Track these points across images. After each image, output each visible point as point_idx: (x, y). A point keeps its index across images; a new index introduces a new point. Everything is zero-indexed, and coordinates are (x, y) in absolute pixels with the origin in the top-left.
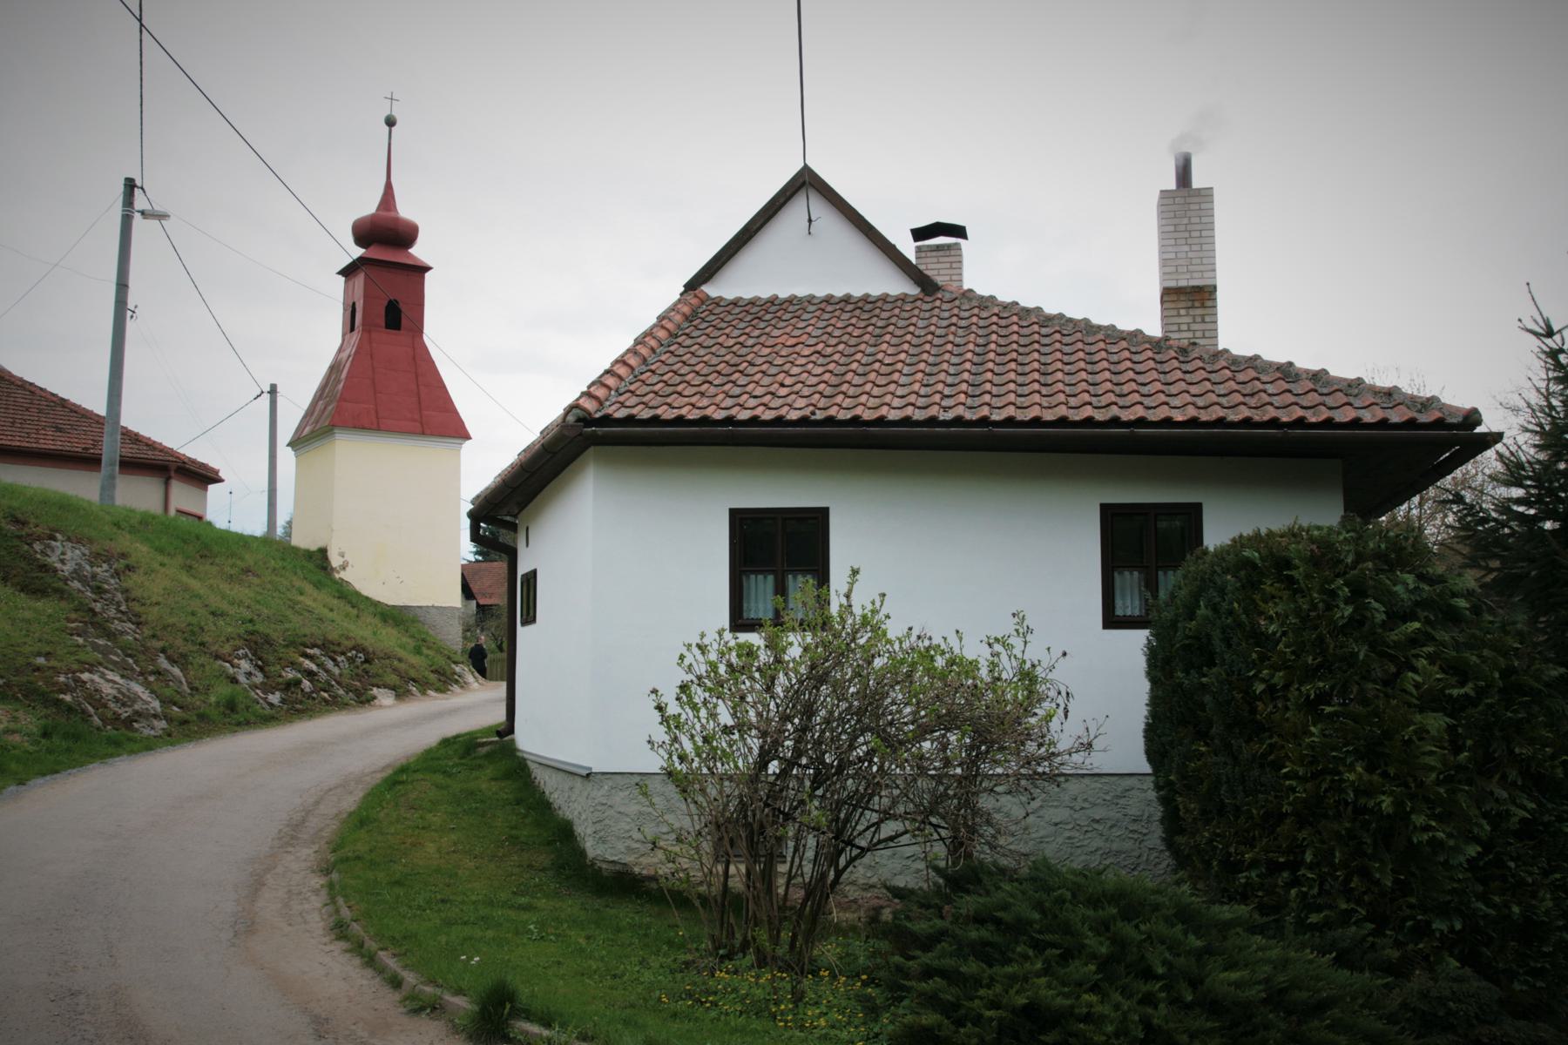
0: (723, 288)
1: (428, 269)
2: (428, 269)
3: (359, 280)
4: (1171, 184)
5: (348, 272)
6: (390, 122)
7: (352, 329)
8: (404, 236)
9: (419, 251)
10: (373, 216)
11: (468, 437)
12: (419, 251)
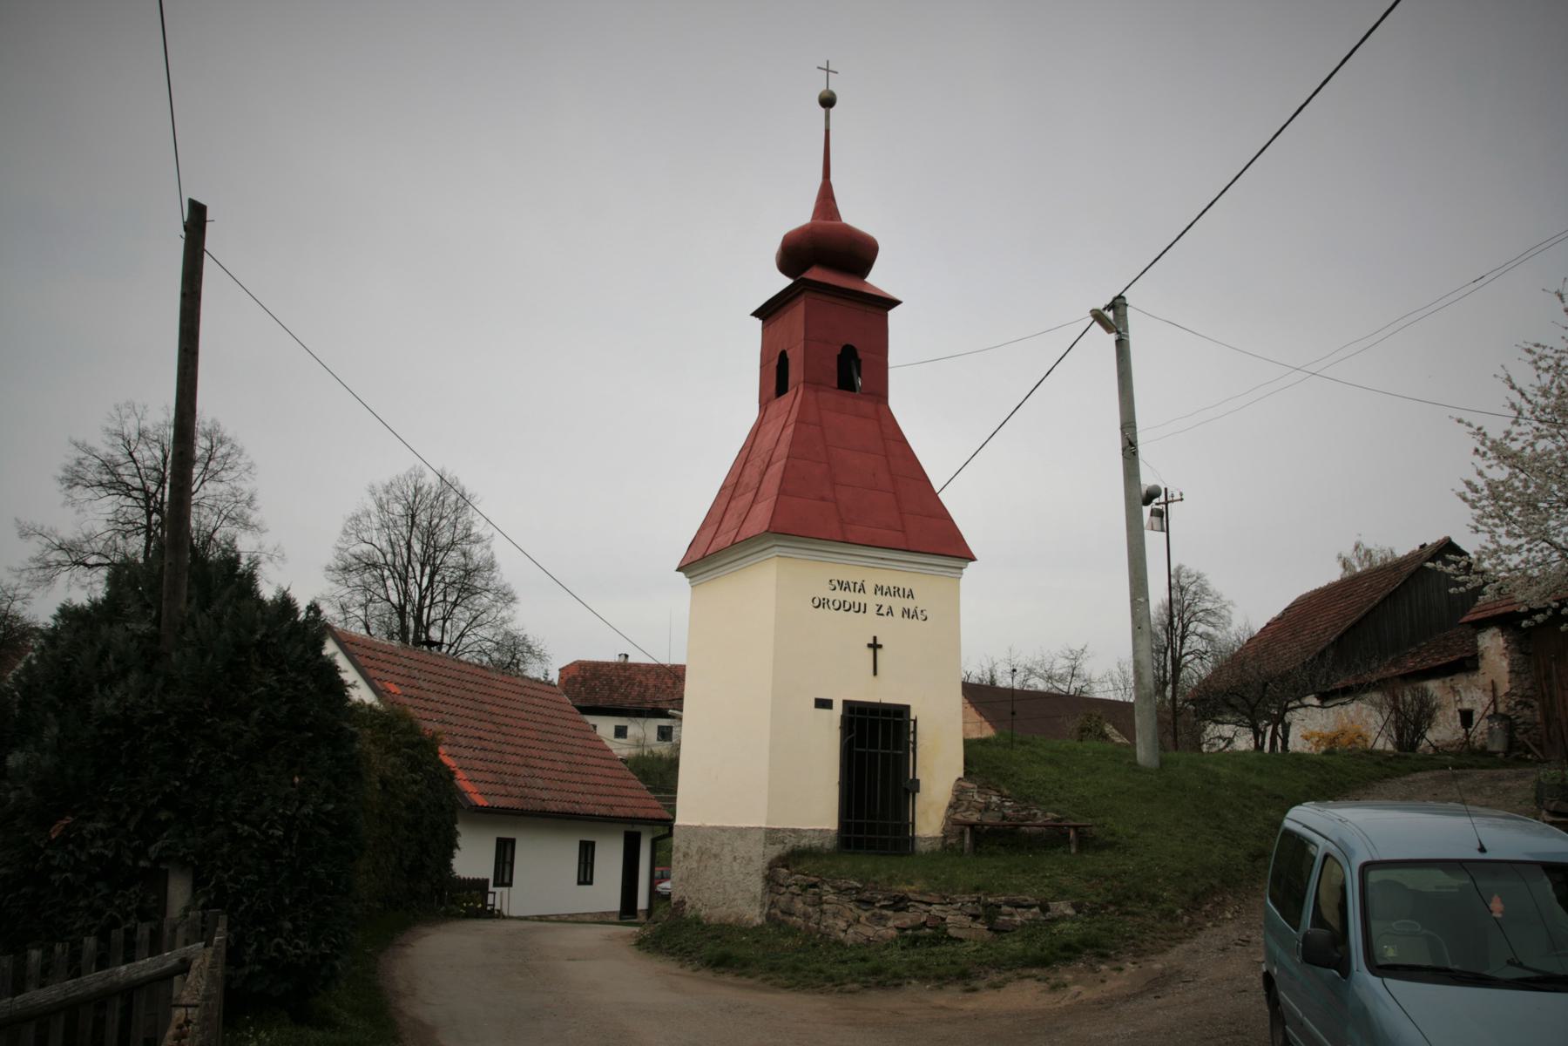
1: (895, 303)
2: (895, 303)
5: (766, 313)
6: (828, 102)
7: (782, 388)
8: (856, 253)
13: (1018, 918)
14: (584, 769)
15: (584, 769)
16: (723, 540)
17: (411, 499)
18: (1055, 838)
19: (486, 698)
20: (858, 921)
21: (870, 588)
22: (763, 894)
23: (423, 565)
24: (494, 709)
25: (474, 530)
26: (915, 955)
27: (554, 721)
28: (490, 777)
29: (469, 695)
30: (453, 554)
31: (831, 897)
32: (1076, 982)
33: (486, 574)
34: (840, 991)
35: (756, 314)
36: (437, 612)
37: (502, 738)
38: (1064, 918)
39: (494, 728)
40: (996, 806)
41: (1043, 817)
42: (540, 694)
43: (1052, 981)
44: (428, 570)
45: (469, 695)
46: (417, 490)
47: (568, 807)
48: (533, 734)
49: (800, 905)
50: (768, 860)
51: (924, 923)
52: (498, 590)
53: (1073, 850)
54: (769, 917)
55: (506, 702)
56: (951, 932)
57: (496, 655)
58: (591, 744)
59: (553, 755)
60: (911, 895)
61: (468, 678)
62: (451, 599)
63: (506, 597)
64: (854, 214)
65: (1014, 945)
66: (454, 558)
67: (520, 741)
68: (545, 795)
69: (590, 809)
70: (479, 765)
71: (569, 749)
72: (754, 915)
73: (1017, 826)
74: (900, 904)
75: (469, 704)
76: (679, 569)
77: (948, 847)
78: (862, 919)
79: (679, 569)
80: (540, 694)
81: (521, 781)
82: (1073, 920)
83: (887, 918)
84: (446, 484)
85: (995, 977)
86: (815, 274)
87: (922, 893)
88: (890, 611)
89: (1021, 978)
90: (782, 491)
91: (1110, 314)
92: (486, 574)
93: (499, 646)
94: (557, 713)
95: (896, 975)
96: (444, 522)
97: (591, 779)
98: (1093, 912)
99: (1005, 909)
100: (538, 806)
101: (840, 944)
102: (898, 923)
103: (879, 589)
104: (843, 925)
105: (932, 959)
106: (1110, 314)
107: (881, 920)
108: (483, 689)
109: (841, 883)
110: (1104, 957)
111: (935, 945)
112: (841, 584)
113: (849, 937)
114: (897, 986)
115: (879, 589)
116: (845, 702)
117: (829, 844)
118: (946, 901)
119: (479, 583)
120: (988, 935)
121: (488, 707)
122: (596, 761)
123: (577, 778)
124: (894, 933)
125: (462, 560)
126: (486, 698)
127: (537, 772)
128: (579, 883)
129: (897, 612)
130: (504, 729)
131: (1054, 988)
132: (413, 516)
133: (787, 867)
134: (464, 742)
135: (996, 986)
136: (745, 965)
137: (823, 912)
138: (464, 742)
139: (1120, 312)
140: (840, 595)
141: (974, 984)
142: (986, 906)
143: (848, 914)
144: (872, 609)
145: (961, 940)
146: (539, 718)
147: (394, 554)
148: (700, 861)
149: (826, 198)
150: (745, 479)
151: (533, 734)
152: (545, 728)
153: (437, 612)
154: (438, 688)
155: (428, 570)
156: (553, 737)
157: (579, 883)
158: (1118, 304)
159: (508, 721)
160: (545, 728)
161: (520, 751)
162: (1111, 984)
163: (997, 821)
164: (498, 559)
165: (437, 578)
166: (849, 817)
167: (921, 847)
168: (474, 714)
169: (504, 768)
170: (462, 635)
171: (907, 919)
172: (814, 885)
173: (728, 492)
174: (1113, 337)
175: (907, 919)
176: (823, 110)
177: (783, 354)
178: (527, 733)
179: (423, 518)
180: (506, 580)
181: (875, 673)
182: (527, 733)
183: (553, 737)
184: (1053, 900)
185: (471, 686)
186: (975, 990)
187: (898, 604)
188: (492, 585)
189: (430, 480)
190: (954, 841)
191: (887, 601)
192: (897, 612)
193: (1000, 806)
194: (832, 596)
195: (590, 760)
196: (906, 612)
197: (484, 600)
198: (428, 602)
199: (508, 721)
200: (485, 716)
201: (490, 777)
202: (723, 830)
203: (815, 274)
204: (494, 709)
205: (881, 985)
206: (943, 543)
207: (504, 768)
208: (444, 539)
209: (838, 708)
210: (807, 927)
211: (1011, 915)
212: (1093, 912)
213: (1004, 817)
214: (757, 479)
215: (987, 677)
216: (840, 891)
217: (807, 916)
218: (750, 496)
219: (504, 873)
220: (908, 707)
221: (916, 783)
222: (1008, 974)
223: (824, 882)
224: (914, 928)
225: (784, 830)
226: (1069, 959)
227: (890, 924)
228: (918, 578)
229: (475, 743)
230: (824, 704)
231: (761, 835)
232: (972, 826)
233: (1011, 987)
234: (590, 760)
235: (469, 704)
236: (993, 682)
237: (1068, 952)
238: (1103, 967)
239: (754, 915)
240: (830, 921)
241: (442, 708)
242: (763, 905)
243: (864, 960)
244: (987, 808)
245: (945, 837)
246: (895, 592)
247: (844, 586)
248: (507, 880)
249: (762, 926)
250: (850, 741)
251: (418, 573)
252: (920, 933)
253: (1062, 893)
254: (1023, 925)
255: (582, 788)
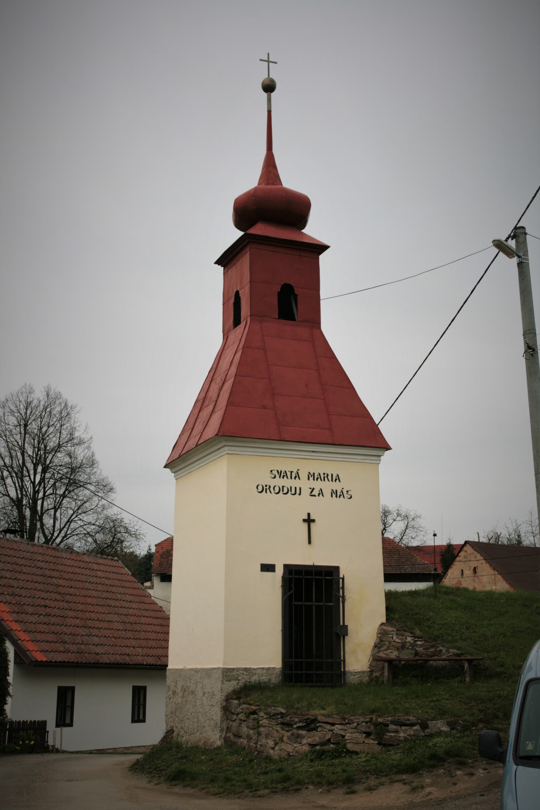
0: (518, 226)
1: (325, 248)
2: (325, 248)
3: (244, 262)
4: (346, 637)
5: (226, 260)
6: (269, 87)
7: (237, 322)
8: (296, 210)
9: (313, 230)
10: (255, 189)
11: (387, 448)
12: (313, 230)
13: (402, 735)
14: (137, 627)
15: (137, 627)
16: (192, 443)
17: (23, 412)
18: (453, 670)
19: (55, 574)
20: (281, 740)
21: (303, 475)
22: (222, 721)
23: (35, 466)
24: (61, 582)
25: (77, 434)
26: (318, 766)
27: (114, 589)
28: (51, 637)
29: (39, 572)
30: (59, 455)
31: (264, 722)
32: (432, 785)
33: (88, 470)
34: (253, 796)
35: (218, 262)
36: (49, 503)
37: (65, 605)
38: (440, 733)
39: (59, 597)
40: (409, 645)
41: (447, 652)
42: (103, 568)
43: (414, 784)
44: (40, 468)
45: (39, 572)
46: (28, 405)
47: (119, 659)
48: (94, 601)
49: (245, 729)
50: (225, 694)
51: (329, 740)
52: (98, 483)
53: (468, 679)
54: (226, 740)
55: (72, 576)
56: (349, 746)
57: (99, 537)
58: (146, 606)
59: (110, 617)
60: (320, 718)
61: (40, 557)
62: (60, 492)
63: (106, 488)
64: (293, 179)
65: (395, 756)
66: (61, 458)
67: (81, 607)
68: (99, 650)
69: (139, 660)
70: (42, 628)
71: (124, 611)
72: (215, 738)
73: (427, 661)
74: (311, 725)
75: (39, 579)
76: (165, 467)
77: (372, 680)
78: (285, 739)
79: (165, 467)
80: (103, 568)
81: (79, 639)
82: (447, 735)
83: (303, 737)
84: (52, 398)
85: (372, 782)
86: (259, 229)
87: (329, 716)
88: (321, 493)
89: (393, 782)
90: (230, 403)
91: (512, 243)
92: (88, 470)
93: (102, 528)
94: (117, 583)
95: (300, 783)
96: (51, 429)
97: (142, 635)
98: (465, 728)
99: (392, 727)
100: (91, 659)
101: (269, 759)
102: (310, 740)
103: (311, 476)
104: (271, 743)
105: (331, 769)
106: (512, 243)
107: (297, 738)
108: (52, 566)
109: (272, 710)
110: (462, 764)
111: (336, 757)
112: (279, 473)
113: (275, 754)
114: (297, 790)
115: (311, 476)
116: (285, 566)
117: (275, 679)
118: (345, 722)
119: (82, 477)
120: (377, 748)
121: (55, 581)
122: (149, 620)
123: (129, 634)
124: (306, 748)
125: (67, 459)
126: (55, 574)
127: (94, 632)
128: (133, 721)
129: (327, 493)
130: (68, 598)
131: (414, 790)
132: (26, 426)
133: (238, 698)
134: (30, 610)
135: (370, 789)
136: (193, 779)
137: (259, 734)
138: (30, 610)
139: (521, 239)
140: (280, 482)
141: (356, 787)
142: (377, 725)
143: (275, 734)
144: (306, 492)
145: (356, 753)
146: (100, 588)
147: (11, 457)
148: (183, 697)
149: (270, 164)
150: (211, 393)
151: (94, 601)
152: (106, 595)
153: (49, 503)
154: (10, 567)
155: (40, 468)
156: (112, 603)
157: (133, 721)
158: (518, 233)
159: (72, 591)
160: (106, 595)
161: (80, 615)
162: (460, 786)
163: (411, 657)
164: (97, 457)
165: (48, 475)
166: (291, 657)
167: (352, 679)
168: (42, 587)
169: (65, 629)
170: (69, 521)
171: (316, 737)
172: (254, 713)
173: (199, 405)
174: (515, 260)
175: (316, 737)
176: (265, 95)
177: (237, 293)
178: (89, 600)
179: (33, 427)
180: (105, 474)
181: (310, 542)
182: (89, 600)
183: (112, 603)
184: (433, 719)
185: (42, 565)
186: (353, 792)
187: (327, 486)
188: (93, 479)
189: (39, 395)
190: (377, 674)
191: (318, 485)
192: (327, 493)
193: (413, 645)
194: (272, 483)
195: (143, 620)
196: (334, 493)
197: (83, 493)
198: (41, 495)
199: (72, 591)
200: (51, 588)
201: (51, 637)
202: (196, 671)
203: (259, 229)
204: (61, 582)
205: (285, 790)
206: (364, 436)
207: (65, 629)
208: (51, 445)
209: (280, 571)
210: (249, 746)
211: (397, 732)
212: (465, 728)
213: (416, 654)
214: (216, 395)
215: (514, 536)
216: (271, 716)
217: (249, 738)
218: (211, 407)
219: (65, 715)
220: (337, 568)
221: (345, 627)
222: (384, 779)
223: (260, 710)
224: (322, 744)
225: (238, 669)
226: (433, 767)
227: (304, 741)
228: (345, 466)
229: (42, 611)
230: (268, 568)
231: (219, 674)
232: (390, 662)
233: (382, 790)
234: (143, 620)
235: (39, 579)
236: (519, 542)
237: (436, 760)
238: (459, 773)
239: (215, 738)
240: (264, 741)
241: (12, 582)
242: (222, 730)
243: (280, 771)
244: (403, 647)
245: (371, 672)
246: (325, 477)
247: (282, 474)
248: (68, 721)
249: (219, 748)
250: (290, 597)
251: (32, 472)
252: (326, 748)
253: (442, 714)
254: (406, 740)
255: (134, 643)
